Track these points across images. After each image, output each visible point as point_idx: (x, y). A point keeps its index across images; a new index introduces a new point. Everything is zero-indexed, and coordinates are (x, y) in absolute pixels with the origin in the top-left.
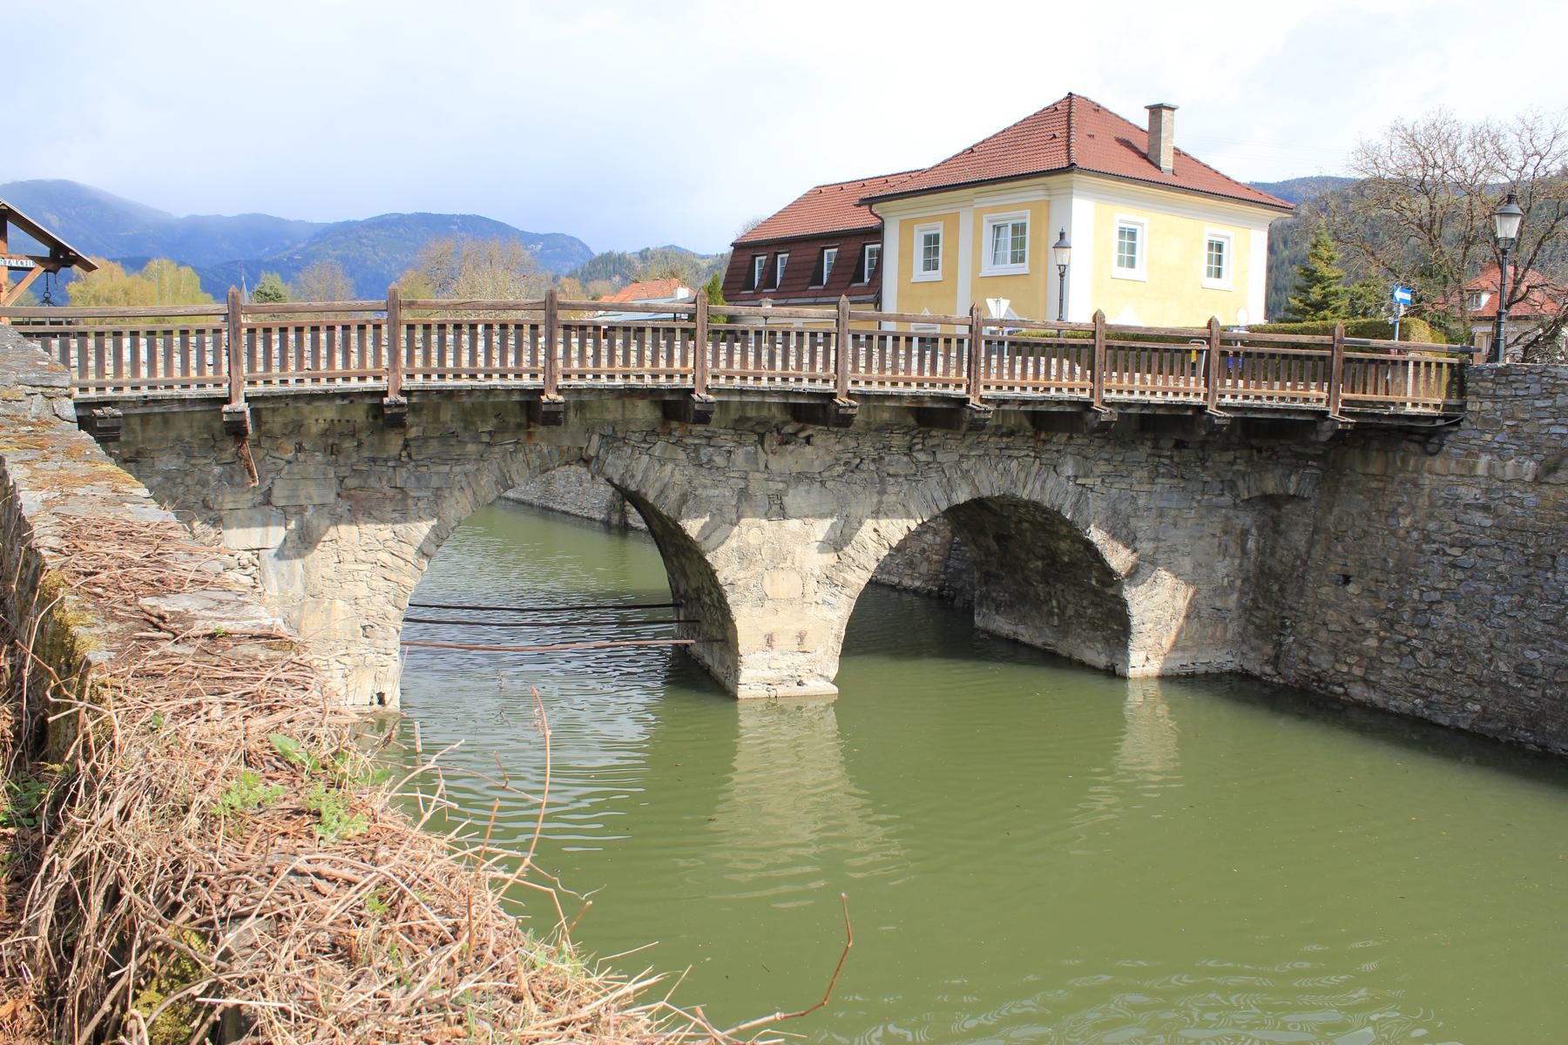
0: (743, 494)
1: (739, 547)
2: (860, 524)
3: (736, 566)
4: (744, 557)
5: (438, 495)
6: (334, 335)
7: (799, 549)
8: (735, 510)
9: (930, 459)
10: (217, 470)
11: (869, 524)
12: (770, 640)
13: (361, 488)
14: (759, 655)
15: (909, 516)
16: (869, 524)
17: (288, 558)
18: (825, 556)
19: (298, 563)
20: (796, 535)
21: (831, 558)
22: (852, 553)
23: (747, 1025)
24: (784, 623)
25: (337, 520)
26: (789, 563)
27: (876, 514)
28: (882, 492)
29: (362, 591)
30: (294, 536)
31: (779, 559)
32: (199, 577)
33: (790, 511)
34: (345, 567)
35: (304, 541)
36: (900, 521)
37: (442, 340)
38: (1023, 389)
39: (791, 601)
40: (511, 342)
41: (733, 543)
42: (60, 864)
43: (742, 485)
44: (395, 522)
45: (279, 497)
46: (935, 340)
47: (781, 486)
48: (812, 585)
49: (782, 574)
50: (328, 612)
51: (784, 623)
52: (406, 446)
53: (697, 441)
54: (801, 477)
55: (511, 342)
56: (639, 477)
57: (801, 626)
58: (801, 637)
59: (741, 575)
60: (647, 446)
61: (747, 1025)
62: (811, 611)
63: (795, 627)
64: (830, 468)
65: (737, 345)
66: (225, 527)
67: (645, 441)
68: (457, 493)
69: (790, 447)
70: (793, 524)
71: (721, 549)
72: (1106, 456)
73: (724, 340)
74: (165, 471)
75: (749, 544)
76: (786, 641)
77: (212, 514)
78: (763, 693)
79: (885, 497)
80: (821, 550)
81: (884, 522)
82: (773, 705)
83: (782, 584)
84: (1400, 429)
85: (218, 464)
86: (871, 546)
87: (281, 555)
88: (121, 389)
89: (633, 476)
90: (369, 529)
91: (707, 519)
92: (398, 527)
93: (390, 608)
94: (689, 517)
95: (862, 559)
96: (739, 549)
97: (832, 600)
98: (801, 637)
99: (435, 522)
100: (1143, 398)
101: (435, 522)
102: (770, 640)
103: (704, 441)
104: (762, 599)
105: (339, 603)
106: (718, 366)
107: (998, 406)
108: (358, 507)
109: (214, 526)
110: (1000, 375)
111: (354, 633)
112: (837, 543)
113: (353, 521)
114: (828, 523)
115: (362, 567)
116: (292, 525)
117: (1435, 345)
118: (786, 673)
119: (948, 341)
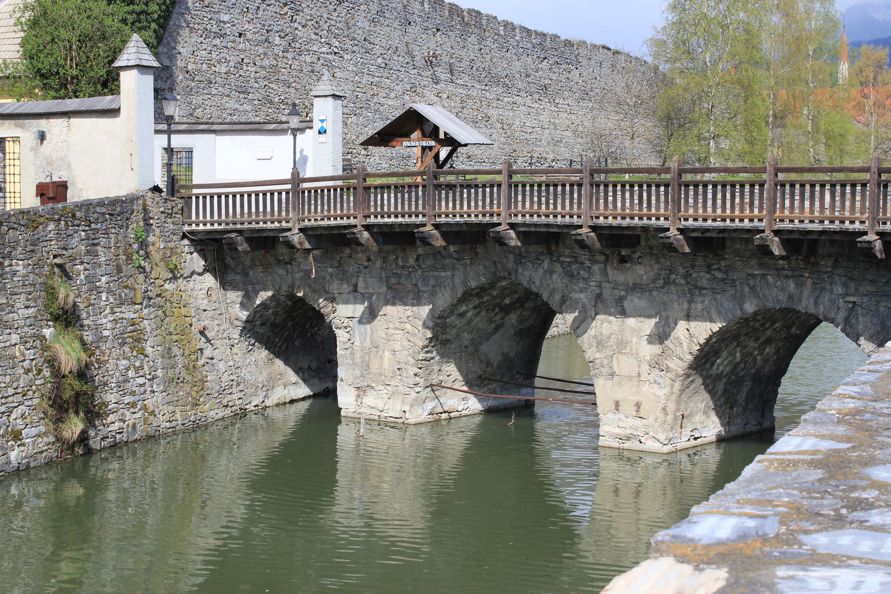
0: (599, 297)
1: (595, 335)
2: (676, 324)
3: (594, 349)
4: (600, 344)
5: (434, 293)
6: (804, 190)
7: (634, 340)
8: (593, 309)
9: (725, 277)
10: (330, 270)
11: (682, 325)
12: (617, 404)
13: (398, 284)
14: (610, 416)
15: (712, 321)
16: (682, 325)
17: (364, 324)
18: (654, 346)
19: (368, 326)
20: (633, 330)
21: (656, 349)
22: (671, 346)
24: (627, 394)
25: (387, 303)
26: (628, 350)
27: (688, 318)
28: (690, 302)
29: (397, 347)
30: (367, 311)
31: (622, 345)
33: (628, 311)
34: (391, 331)
35: (371, 315)
36: (704, 324)
37: (555, 191)
38: (801, 221)
39: (630, 378)
40: (807, 195)
41: (591, 332)
43: (598, 291)
44: (413, 305)
45: (361, 288)
46: (403, 187)
47: (623, 293)
48: (645, 368)
49: (624, 358)
50: (382, 358)
51: (627, 394)
52: (417, 259)
53: (568, 260)
54: (636, 288)
55: (807, 195)
56: (538, 284)
57: (637, 398)
58: (638, 405)
59: (598, 356)
60: (540, 262)
62: (645, 388)
64: (654, 282)
65: (473, 190)
66: (338, 304)
67: (538, 259)
68: (443, 290)
69: (628, 265)
70: (631, 321)
71: (586, 336)
72: (871, 278)
73: (451, 189)
74: (306, 270)
75: (602, 334)
76: (628, 408)
77: (329, 295)
78: (615, 444)
79: (693, 304)
80: (650, 342)
81: (693, 324)
82: (621, 455)
83: (624, 365)
85: (331, 267)
86: (685, 342)
87: (360, 322)
88: (243, 224)
89: (534, 283)
90: (401, 308)
91: (577, 314)
92: (415, 308)
93: (410, 358)
95: (678, 351)
96: (595, 337)
98: (638, 405)
99: (431, 306)
100: (802, 226)
101: (431, 306)
102: (617, 404)
103: (572, 260)
104: (612, 375)
105: (387, 353)
106: (783, 212)
107: (703, 233)
108: (397, 297)
109: (331, 302)
110: (696, 210)
112: (660, 336)
113: (394, 304)
114: (653, 321)
115: (397, 332)
116: (366, 304)
118: (629, 432)
119: (532, 186)
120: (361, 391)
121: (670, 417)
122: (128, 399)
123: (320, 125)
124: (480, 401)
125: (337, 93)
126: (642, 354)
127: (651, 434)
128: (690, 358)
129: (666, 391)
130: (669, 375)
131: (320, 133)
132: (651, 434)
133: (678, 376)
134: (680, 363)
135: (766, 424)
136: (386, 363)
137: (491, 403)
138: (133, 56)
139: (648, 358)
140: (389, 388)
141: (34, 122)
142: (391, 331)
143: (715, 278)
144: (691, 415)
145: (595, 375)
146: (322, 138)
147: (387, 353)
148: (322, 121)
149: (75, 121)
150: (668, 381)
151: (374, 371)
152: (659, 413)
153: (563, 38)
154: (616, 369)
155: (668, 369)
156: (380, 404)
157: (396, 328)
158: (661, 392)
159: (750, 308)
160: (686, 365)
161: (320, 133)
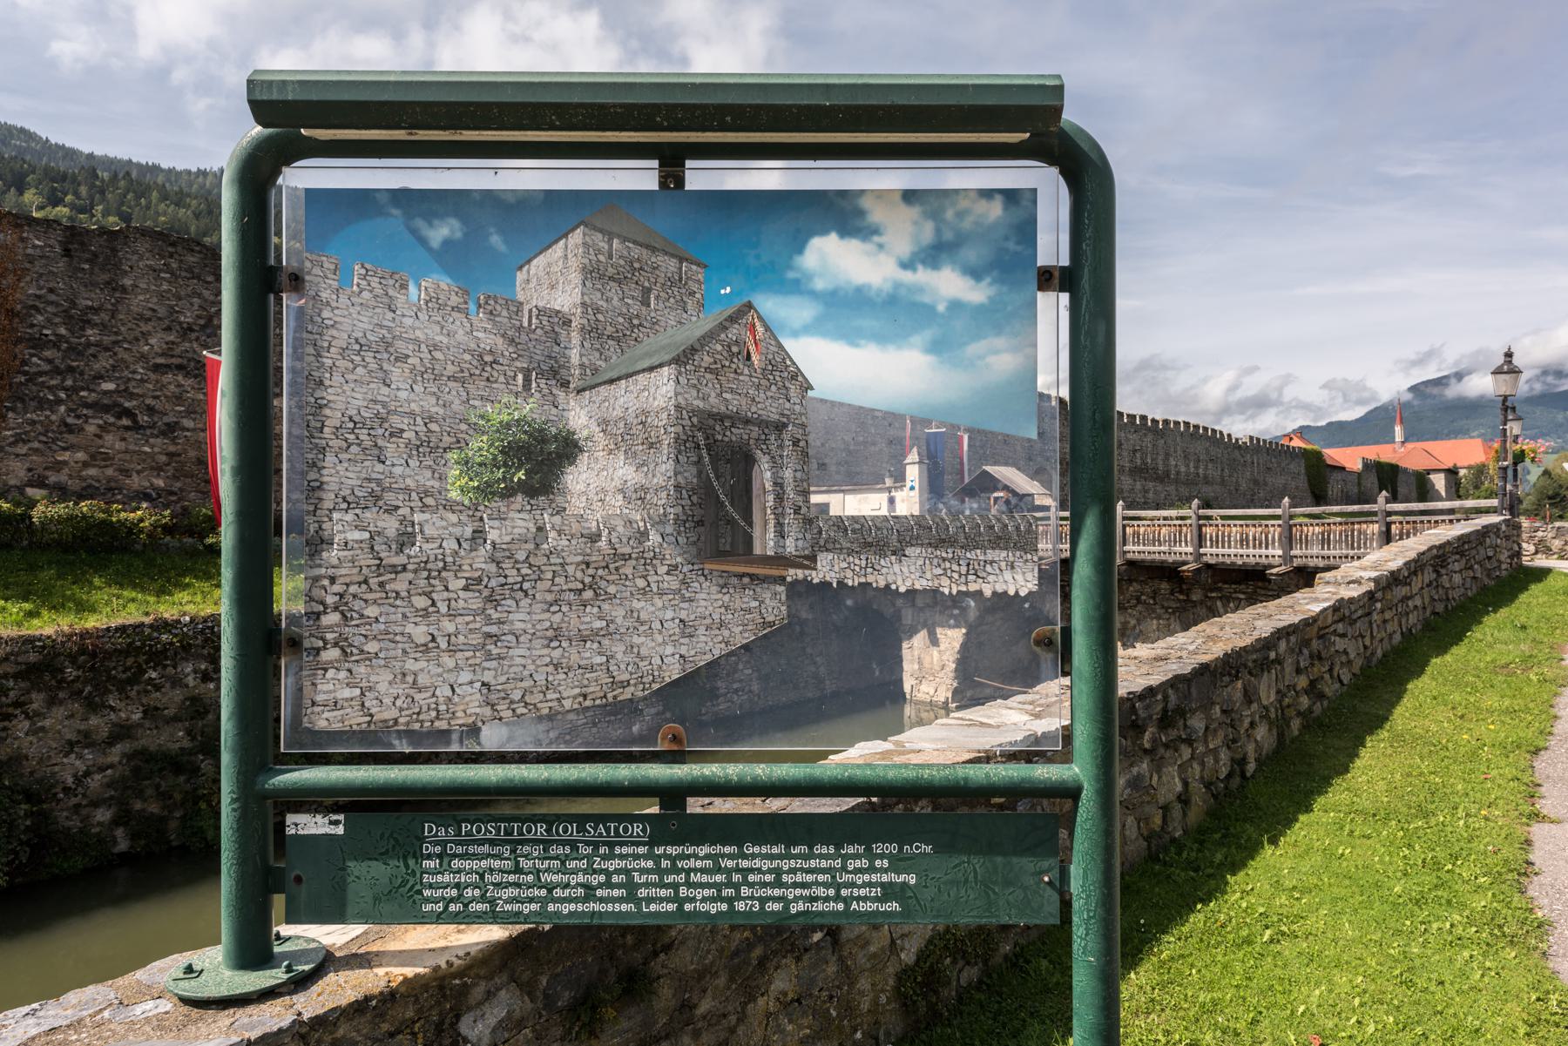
120: (920, 680)
122: (735, 686)
146: (912, 493)
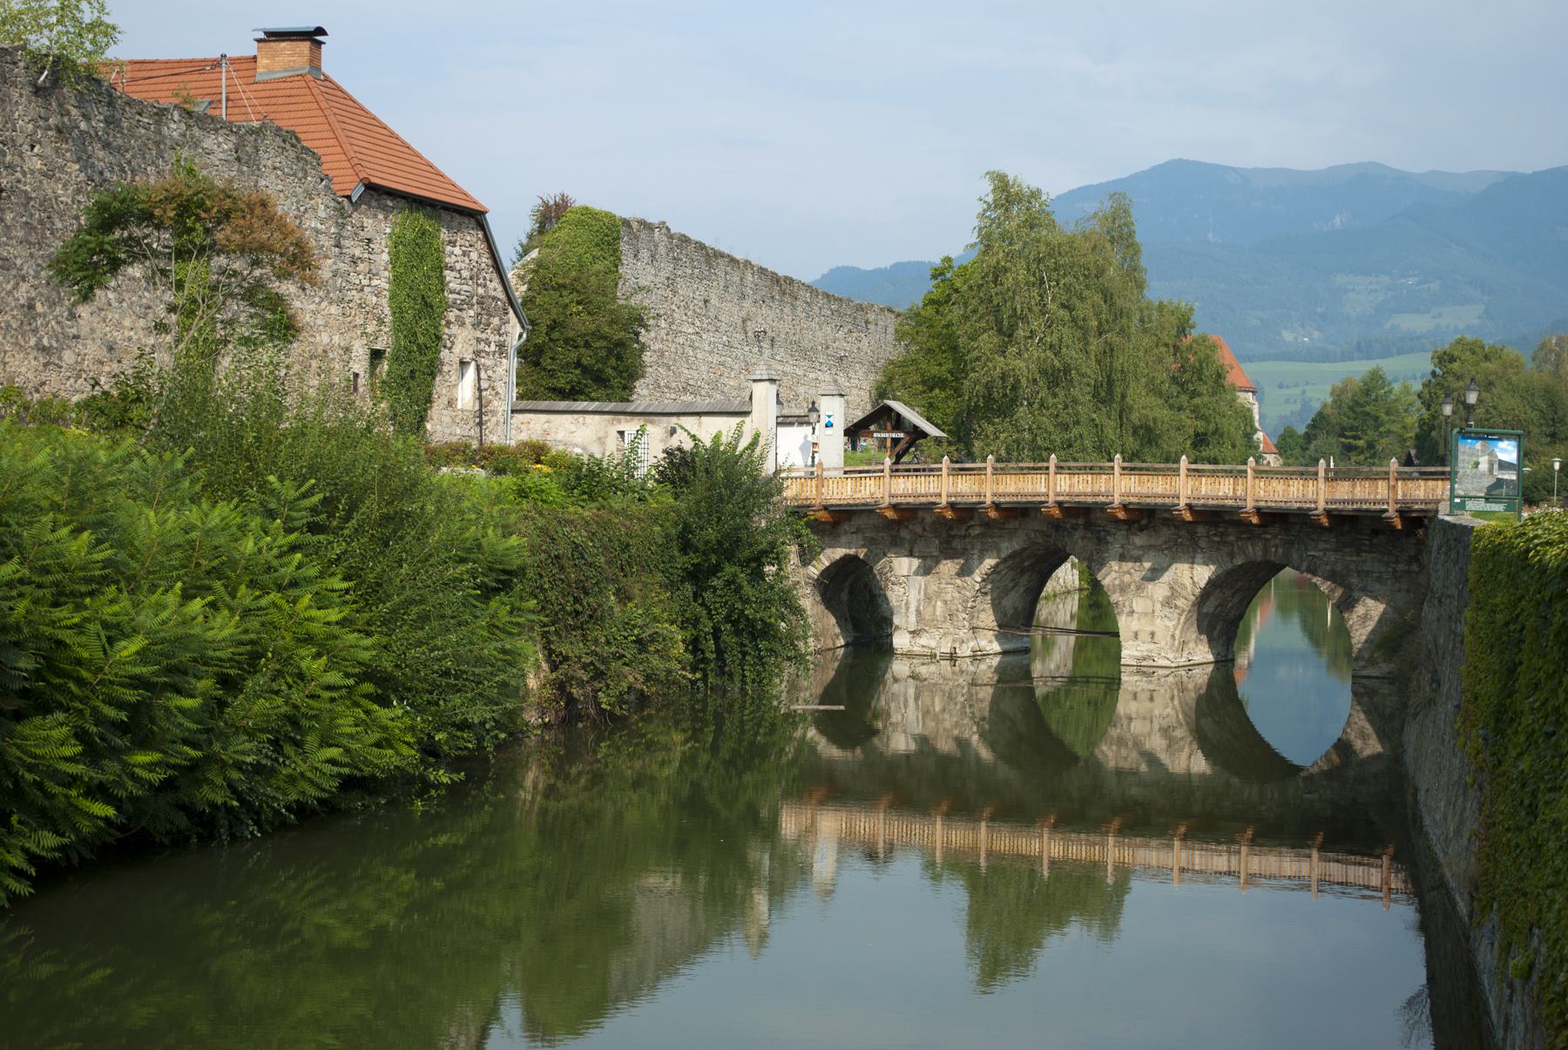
12: (1136, 635)
14: (1131, 643)
23: (835, 708)
29: (949, 597)
32: (140, 431)
34: (943, 586)
39: (1146, 614)
42: (1112, 851)
48: (1158, 606)
49: (1142, 600)
50: (934, 607)
58: (1153, 634)
61: (835, 708)
63: (1149, 629)
76: (1144, 636)
84: (868, 510)
94: (1385, 609)
95: (1184, 593)
97: (1169, 615)
104: (1132, 612)
105: (939, 603)
111: (945, 618)
117: (908, 488)
118: (1145, 654)
121: (1176, 643)
123: (827, 419)
124: (1000, 644)
125: (774, 378)
126: (1155, 597)
127: (1163, 654)
128: (1193, 598)
129: (1174, 623)
130: (1177, 611)
131: (827, 426)
132: (1163, 654)
133: (1183, 611)
134: (1185, 602)
135: (1230, 657)
136: (939, 611)
137: (1008, 646)
138: (764, 372)
139: (1160, 599)
140: (941, 630)
141: (665, 419)
142: (943, 586)
143: (1213, 541)
144: (1188, 642)
145: (1119, 613)
146: (829, 431)
147: (939, 603)
148: (829, 417)
149: (704, 419)
150: (1176, 615)
151: (927, 618)
152: (1169, 638)
153: (578, 204)
154: (1135, 608)
155: (1176, 607)
156: (933, 644)
157: (947, 584)
158: (1170, 624)
159: (1239, 561)
160: (1190, 603)
161: (827, 426)
